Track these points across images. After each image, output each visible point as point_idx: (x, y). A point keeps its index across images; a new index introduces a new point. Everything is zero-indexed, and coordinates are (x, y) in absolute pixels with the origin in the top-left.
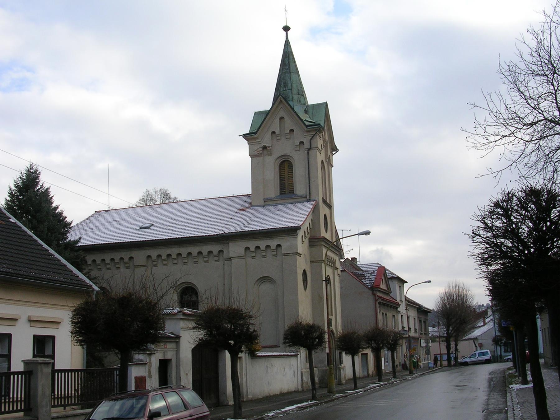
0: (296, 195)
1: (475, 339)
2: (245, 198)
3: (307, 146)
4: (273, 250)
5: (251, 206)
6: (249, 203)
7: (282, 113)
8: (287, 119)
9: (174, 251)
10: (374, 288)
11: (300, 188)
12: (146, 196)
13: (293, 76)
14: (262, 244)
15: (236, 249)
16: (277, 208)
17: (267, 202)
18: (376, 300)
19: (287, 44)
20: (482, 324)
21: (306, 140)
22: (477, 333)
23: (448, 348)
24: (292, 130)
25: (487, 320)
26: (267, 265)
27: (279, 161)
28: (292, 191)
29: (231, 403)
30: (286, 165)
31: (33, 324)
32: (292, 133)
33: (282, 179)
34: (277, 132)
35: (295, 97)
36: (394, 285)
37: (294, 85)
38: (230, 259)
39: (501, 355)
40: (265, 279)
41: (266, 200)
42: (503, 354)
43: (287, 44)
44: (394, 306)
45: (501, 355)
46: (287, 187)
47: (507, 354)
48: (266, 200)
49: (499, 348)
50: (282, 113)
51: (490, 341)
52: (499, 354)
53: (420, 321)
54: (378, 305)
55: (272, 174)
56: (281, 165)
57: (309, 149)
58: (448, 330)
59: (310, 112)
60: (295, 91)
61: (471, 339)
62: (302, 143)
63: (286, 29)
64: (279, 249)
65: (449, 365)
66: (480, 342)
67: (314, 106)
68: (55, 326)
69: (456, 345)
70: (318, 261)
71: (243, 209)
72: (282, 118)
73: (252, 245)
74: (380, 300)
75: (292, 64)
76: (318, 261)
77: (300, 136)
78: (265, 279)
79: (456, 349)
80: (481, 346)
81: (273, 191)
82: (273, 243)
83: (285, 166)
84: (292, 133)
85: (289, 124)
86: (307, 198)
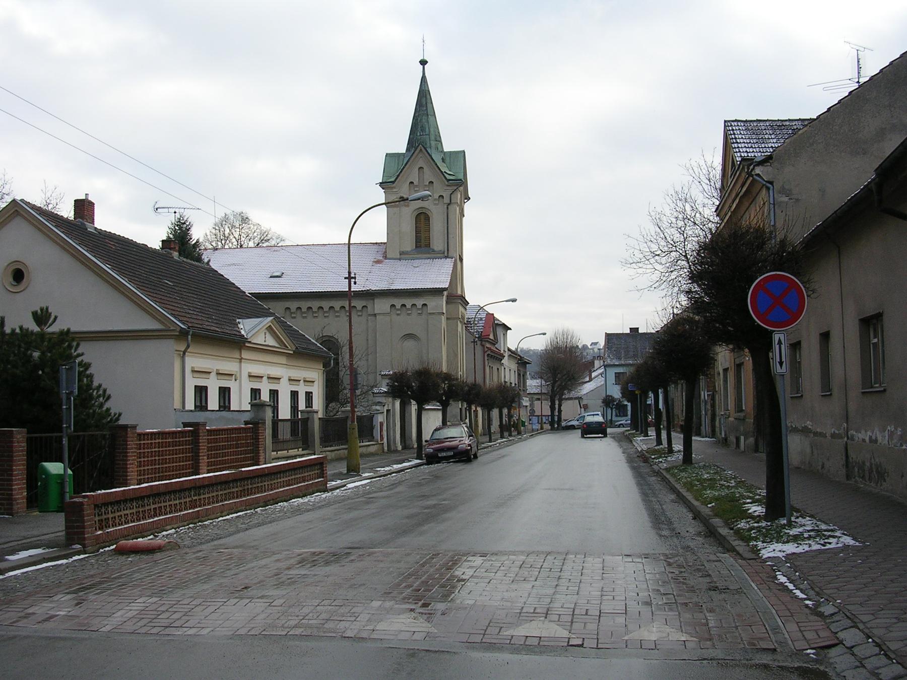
0: (433, 251)
1: (580, 399)
2: (376, 246)
3: (447, 200)
4: (419, 309)
5: (386, 258)
6: (384, 253)
7: (421, 163)
8: (426, 169)
9: (315, 304)
10: (482, 338)
11: (437, 243)
12: (808, 450)
13: (431, 119)
14: (409, 302)
15: (382, 306)
16: (417, 262)
17: (403, 255)
18: (485, 352)
19: (424, 80)
20: (587, 379)
21: (446, 195)
22: (587, 388)
23: (552, 408)
24: (431, 182)
25: (594, 375)
26: (412, 323)
27: (416, 213)
28: (428, 245)
29: (416, 446)
30: (422, 217)
31: (252, 379)
32: (426, 181)
33: (418, 232)
34: (416, 183)
35: (433, 143)
36: (500, 331)
37: (432, 130)
38: (375, 315)
39: (611, 420)
40: (410, 336)
41: (402, 253)
42: (614, 418)
43: (424, 80)
44: (497, 357)
45: (611, 420)
46: (423, 241)
47: (619, 419)
48: (402, 253)
49: (609, 411)
50: (421, 163)
51: (600, 402)
52: (609, 418)
53: (519, 375)
54: (486, 358)
55: (408, 227)
56: (418, 217)
57: (449, 204)
58: (553, 387)
59: (447, 160)
60: (433, 137)
61: (576, 398)
62: (442, 196)
63: (423, 63)
64: (425, 308)
65: (553, 429)
66: (584, 402)
67: (451, 153)
68: (259, 380)
69: (560, 405)
70: (454, 319)
71: (378, 262)
72: (421, 168)
73: (398, 302)
74: (489, 352)
75: (429, 105)
76: (454, 319)
77: (440, 189)
78: (410, 336)
79: (560, 411)
80: (586, 407)
81: (409, 244)
82: (419, 302)
83: (422, 219)
84: (426, 181)
85: (428, 176)
86: (445, 254)
